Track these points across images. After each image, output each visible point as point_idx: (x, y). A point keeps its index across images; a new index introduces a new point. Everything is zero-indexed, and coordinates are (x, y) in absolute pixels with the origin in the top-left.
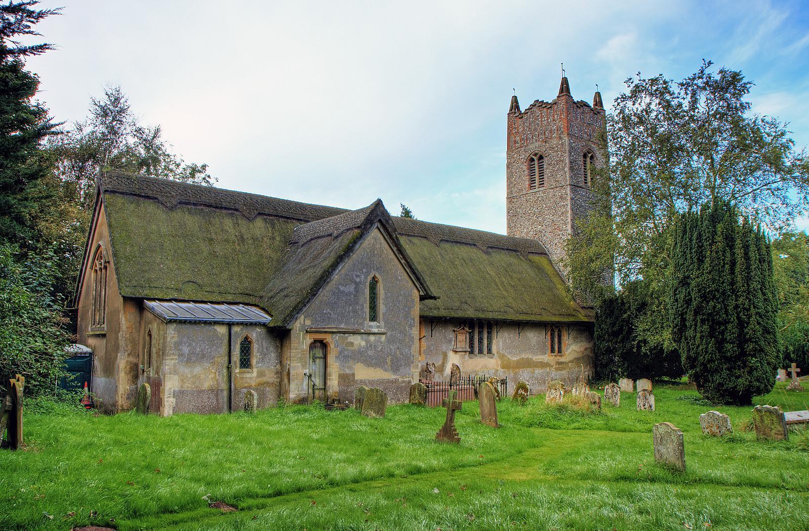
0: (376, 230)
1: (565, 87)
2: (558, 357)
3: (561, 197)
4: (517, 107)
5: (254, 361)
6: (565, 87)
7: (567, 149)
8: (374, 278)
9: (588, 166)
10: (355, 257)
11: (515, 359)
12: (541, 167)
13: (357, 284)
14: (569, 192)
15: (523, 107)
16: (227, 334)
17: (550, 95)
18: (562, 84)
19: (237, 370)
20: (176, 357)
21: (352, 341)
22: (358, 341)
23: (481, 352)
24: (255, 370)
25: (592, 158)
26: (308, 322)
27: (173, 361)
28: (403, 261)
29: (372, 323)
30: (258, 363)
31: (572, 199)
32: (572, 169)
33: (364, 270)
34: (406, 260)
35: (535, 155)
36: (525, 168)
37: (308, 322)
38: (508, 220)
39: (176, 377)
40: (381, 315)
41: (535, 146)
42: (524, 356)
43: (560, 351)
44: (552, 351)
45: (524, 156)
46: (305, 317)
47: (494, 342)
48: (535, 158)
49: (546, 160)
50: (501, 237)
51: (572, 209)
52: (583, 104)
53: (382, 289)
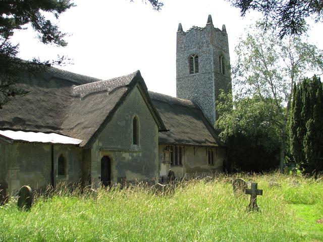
0: (137, 88)
1: (210, 20)
2: (212, 166)
3: (209, 79)
4: (182, 30)
5: (67, 170)
6: (210, 20)
7: (212, 52)
8: (135, 118)
9: (221, 61)
10: (125, 103)
11: (193, 167)
12: (197, 62)
13: (127, 121)
14: (213, 76)
15: (185, 30)
16: (50, 152)
17: (203, 24)
18: (179, 27)
19: (57, 176)
20: (19, 168)
21: (124, 156)
22: (127, 156)
23: (176, 164)
24: (68, 176)
25: (223, 58)
26: (101, 144)
27: (16, 171)
28: (150, 108)
29: (134, 145)
30: (69, 171)
31: (215, 79)
32: (214, 63)
33: (131, 112)
34: (152, 107)
35: (193, 55)
36: (187, 62)
37: (101, 144)
38: (177, 90)
39: (18, 182)
40: (139, 141)
41: (193, 51)
42: (198, 165)
43: (212, 163)
44: (209, 163)
45: (186, 55)
46: (99, 142)
47: (183, 158)
48: (193, 57)
49: (200, 59)
50: (171, 98)
51: (215, 85)
52: (218, 30)
53: (139, 124)
